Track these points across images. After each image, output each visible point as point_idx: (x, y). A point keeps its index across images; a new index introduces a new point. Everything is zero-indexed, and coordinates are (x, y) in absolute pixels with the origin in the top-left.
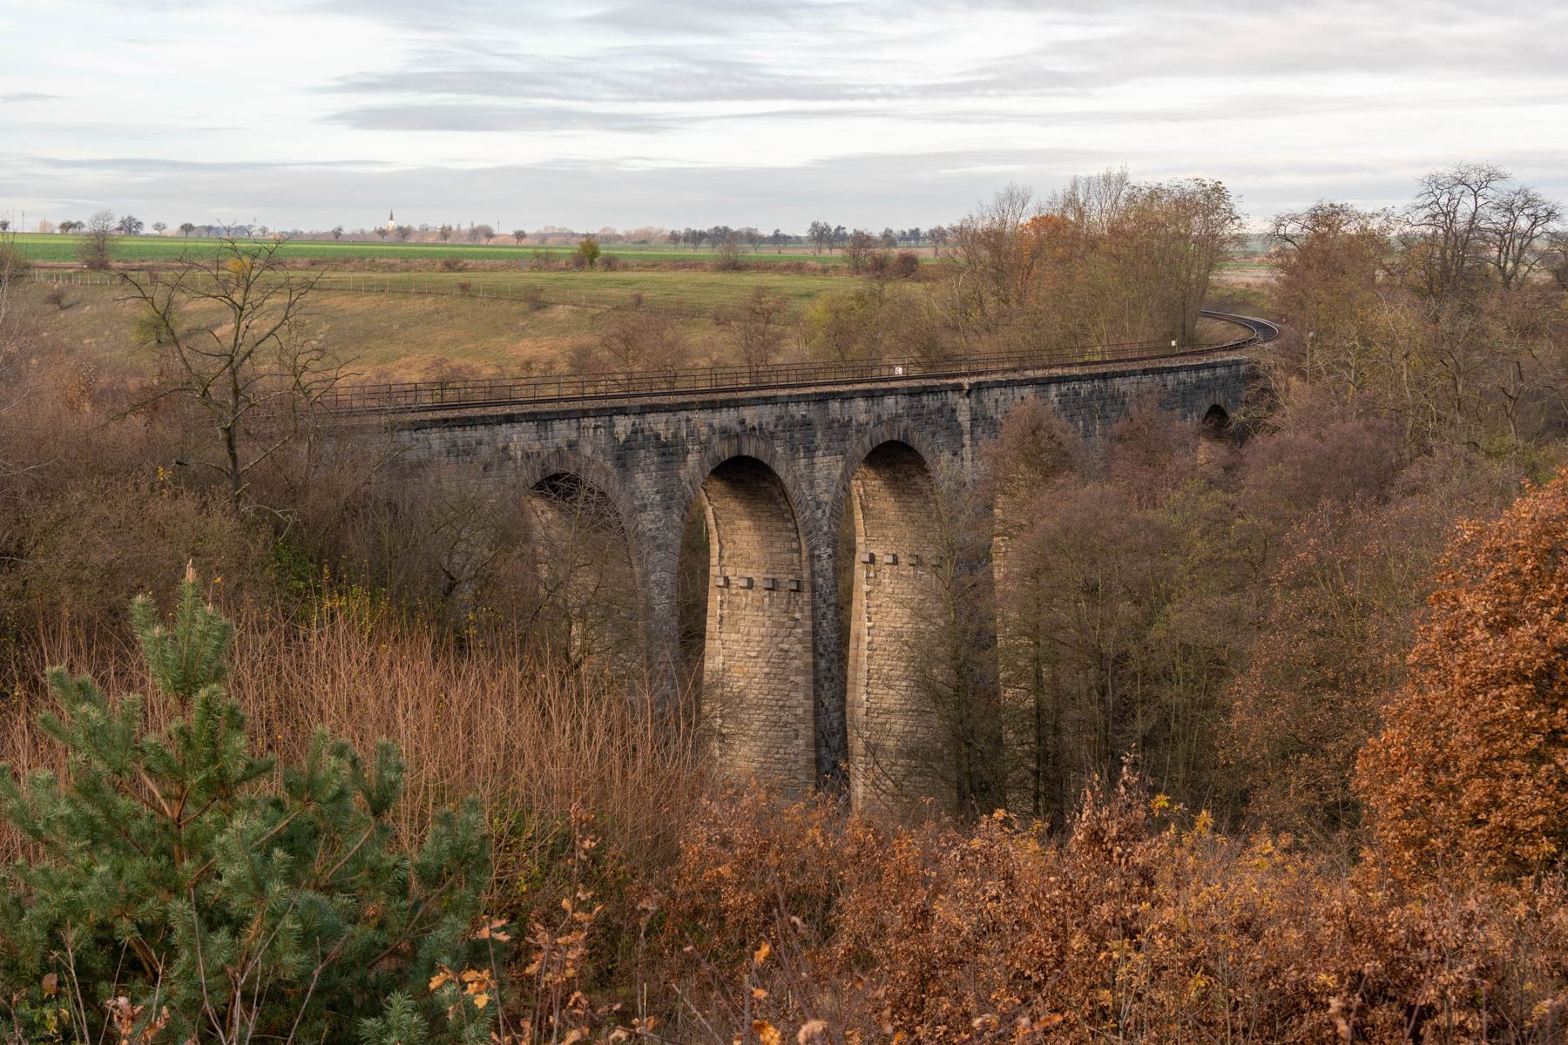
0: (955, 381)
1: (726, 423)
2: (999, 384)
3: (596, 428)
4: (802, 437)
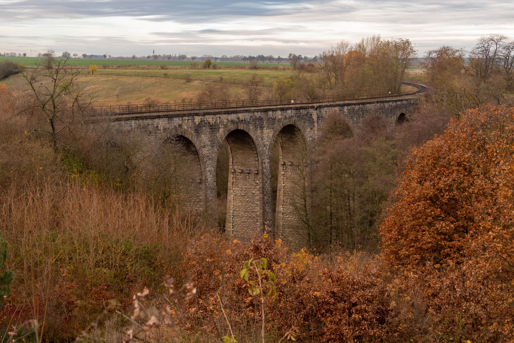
0: (312, 105)
1: (233, 118)
2: (327, 106)
3: (188, 120)
4: (259, 123)
